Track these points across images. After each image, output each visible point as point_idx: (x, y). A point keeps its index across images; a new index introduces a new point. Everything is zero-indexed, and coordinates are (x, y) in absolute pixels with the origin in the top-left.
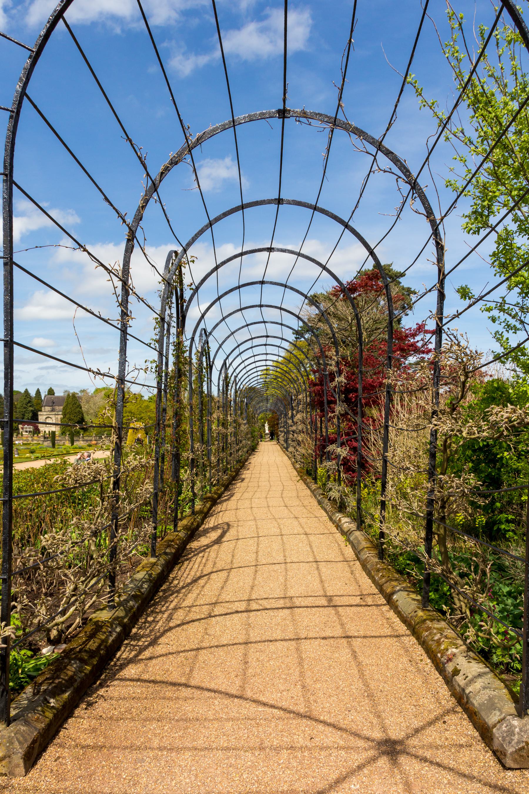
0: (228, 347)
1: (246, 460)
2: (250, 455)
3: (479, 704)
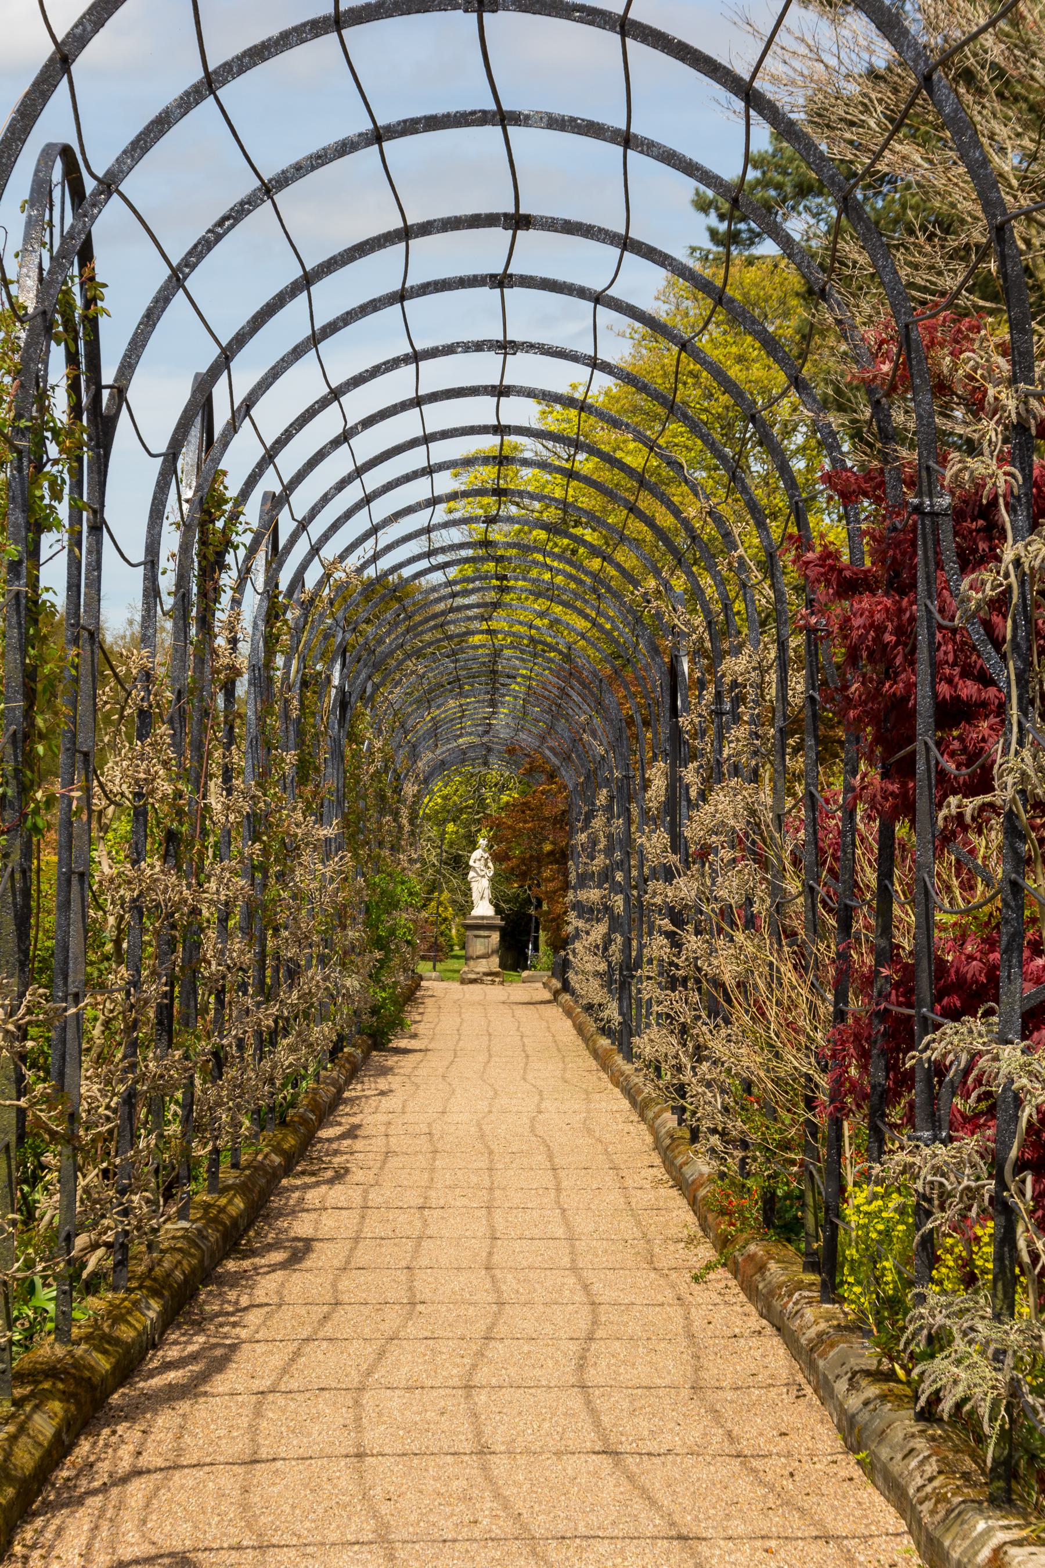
1: (326, 1110)
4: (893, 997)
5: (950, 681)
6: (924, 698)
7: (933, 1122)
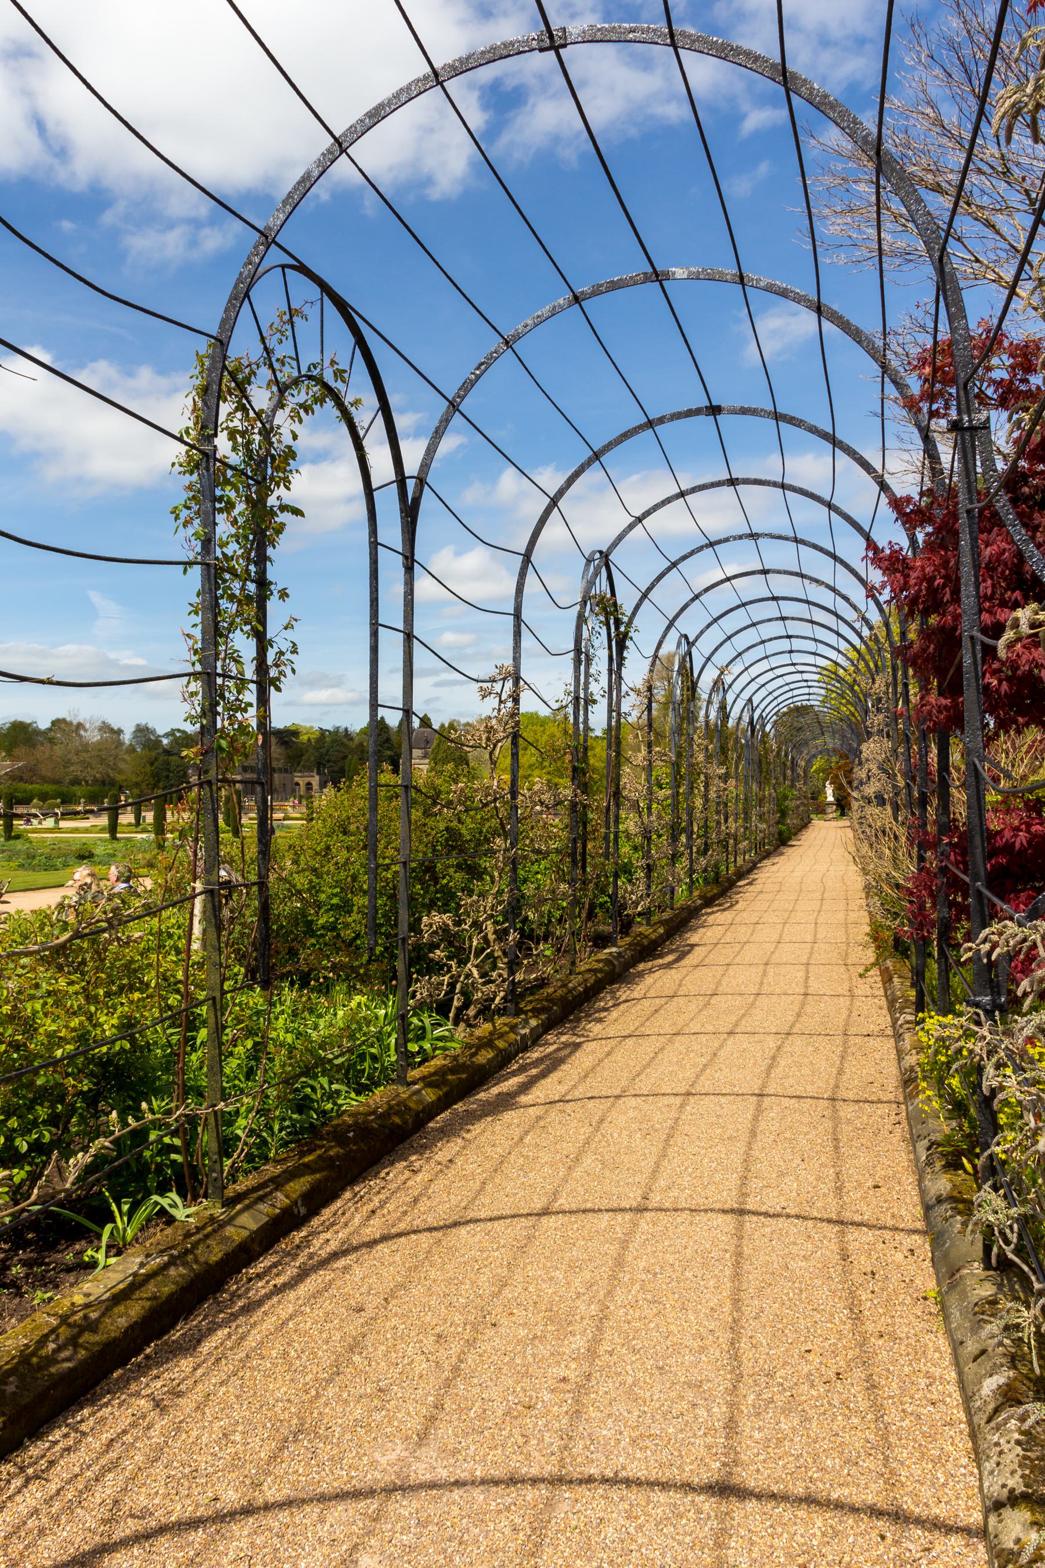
0: (722, 657)
2: (768, 855)
3: (252, 989)
4: (952, 857)
5: (989, 611)
6: (968, 597)
7: (992, 988)
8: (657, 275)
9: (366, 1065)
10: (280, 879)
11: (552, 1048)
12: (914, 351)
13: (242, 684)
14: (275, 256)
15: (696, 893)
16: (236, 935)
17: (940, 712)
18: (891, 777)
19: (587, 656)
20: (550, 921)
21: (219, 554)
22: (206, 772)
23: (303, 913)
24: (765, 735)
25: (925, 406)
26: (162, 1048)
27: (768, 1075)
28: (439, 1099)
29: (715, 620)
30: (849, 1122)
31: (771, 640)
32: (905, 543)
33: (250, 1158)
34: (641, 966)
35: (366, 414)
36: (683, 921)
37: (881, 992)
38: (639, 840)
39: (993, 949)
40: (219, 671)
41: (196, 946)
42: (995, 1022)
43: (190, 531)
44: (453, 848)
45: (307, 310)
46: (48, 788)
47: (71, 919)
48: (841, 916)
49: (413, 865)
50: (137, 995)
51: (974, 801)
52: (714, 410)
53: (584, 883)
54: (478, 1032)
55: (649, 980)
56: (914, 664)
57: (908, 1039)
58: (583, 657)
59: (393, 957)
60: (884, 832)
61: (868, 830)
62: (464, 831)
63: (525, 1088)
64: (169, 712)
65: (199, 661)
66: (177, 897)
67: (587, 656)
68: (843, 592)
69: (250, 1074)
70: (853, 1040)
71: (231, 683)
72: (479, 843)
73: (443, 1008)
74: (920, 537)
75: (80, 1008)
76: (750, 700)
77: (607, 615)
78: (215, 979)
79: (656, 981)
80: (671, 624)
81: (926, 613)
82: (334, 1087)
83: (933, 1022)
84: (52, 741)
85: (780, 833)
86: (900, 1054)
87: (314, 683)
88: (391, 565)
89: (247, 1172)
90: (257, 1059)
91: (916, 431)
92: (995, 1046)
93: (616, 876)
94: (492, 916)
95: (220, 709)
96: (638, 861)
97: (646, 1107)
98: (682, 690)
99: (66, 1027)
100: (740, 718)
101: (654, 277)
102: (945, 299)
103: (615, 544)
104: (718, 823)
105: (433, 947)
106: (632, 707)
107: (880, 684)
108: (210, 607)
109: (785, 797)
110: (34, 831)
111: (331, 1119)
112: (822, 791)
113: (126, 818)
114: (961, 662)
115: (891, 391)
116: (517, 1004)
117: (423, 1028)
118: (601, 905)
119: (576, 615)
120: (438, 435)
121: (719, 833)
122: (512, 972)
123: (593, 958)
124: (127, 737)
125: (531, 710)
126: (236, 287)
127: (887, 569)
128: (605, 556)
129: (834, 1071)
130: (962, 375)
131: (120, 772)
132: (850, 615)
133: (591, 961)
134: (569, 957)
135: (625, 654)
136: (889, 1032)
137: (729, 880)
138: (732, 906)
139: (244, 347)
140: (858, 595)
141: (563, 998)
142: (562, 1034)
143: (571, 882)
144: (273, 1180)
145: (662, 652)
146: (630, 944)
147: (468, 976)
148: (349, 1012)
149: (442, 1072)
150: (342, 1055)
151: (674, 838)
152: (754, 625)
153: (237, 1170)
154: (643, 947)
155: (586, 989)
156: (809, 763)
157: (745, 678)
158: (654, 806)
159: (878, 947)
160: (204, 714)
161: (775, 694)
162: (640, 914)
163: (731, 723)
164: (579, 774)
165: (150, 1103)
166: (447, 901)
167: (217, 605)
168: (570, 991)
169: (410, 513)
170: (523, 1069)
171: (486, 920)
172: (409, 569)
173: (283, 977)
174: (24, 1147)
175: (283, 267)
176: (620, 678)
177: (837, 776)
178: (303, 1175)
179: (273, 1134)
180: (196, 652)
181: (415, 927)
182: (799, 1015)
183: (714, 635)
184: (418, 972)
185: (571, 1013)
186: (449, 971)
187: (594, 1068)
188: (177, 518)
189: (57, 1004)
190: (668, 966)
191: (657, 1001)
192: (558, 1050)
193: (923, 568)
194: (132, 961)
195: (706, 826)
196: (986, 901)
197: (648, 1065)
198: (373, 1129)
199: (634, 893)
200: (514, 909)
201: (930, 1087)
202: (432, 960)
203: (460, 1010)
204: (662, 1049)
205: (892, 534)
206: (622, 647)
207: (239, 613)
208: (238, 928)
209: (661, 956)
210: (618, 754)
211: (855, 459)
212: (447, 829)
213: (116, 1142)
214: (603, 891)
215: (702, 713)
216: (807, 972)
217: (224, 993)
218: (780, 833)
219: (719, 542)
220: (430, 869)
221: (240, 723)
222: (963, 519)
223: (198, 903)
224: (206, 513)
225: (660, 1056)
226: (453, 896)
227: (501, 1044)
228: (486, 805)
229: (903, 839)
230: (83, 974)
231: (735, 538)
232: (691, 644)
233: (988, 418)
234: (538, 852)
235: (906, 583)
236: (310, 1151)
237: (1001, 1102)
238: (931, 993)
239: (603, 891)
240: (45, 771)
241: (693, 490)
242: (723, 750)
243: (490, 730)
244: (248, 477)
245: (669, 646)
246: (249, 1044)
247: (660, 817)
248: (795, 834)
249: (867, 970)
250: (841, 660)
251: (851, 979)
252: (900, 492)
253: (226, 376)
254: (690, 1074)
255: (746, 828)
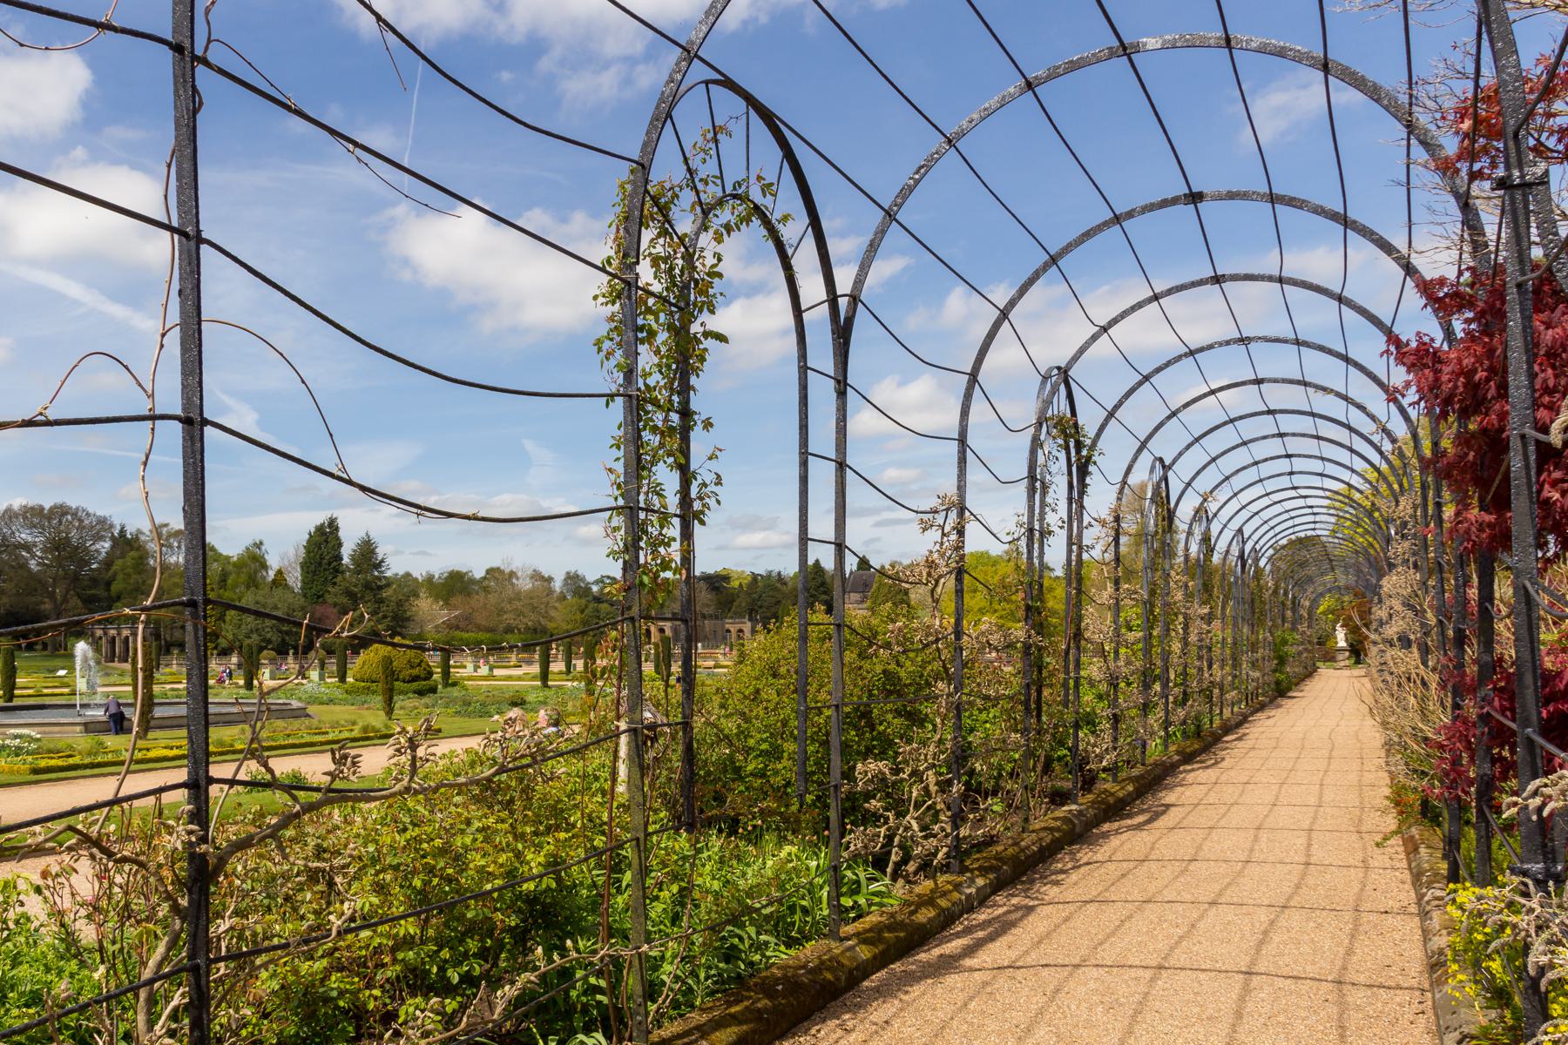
0: (1205, 483)
2: (1262, 707)
4: (1497, 703)
6: (1518, 388)
7: (1545, 855)
8: (1125, 49)
9: (797, 917)
10: (708, 723)
11: (1001, 911)
12: (1449, 103)
13: (664, 518)
14: (698, 72)
15: (1173, 748)
16: (662, 779)
17: (1481, 530)
18: (1419, 613)
19: (1043, 483)
20: (1000, 775)
21: (641, 385)
22: (629, 608)
23: (731, 758)
24: (1259, 572)
25: (1464, 167)
26: (589, 889)
27: (1258, 951)
28: (875, 957)
29: (1197, 440)
30: (1359, 1008)
31: (1266, 460)
32: (1439, 336)
33: (676, 1005)
34: (1106, 827)
35: (794, 229)
36: (1156, 779)
37: (1404, 864)
38: (1103, 687)
39: (1544, 805)
40: (642, 505)
41: (621, 789)
42: (1549, 893)
43: (613, 362)
44: (890, 693)
45: (731, 126)
46: (481, 636)
47: (497, 752)
48: (1353, 777)
49: (847, 709)
50: (562, 835)
51: (1524, 632)
52: (1195, 198)
53: (1039, 733)
54: (918, 889)
55: (1115, 842)
56: (1448, 476)
57: (1436, 919)
58: (1038, 484)
59: (826, 806)
60: (1409, 679)
61: (1389, 678)
62: (903, 674)
63: (970, 951)
64: (590, 554)
65: (622, 495)
66: (603, 737)
67: (1043, 483)
68: (1358, 400)
69: (676, 919)
70: (1365, 917)
71: (654, 518)
72: (920, 688)
73: (880, 863)
74: (1458, 326)
75: (508, 845)
76: (1240, 531)
77: (1066, 437)
78: (639, 819)
79: (1123, 844)
80: (1143, 445)
81: (1464, 414)
82: (763, 938)
83: (1467, 895)
84: (486, 589)
85: (1278, 683)
86: (1426, 934)
87: (748, 525)
88: (822, 391)
89: (671, 1019)
90: (683, 905)
91: (1453, 200)
92: (1547, 920)
93: (1077, 726)
94: (934, 766)
95: (642, 544)
96: (1103, 710)
97: (1109, 979)
98: (1156, 521)
99: (495, 862)
100: (1227, 552)
101: (1121, 52)
102: (1489, 33)
103: (1075, 358)
104: (1200, 669)
105: (868, 796)
106: (1097, 543)
107: (1405, 506)
108: (633, 441)
109: (1285, 642)
110: (470, 678)
111: (759, 971)
112: (1331, 635)
113: (557, 666)
114: (1509, 467)
115: (1419, 154)
116: (962, 862)
117: (858, 882)
118: (1060, 759)
119: (1029, 439)
120: (873, 248)
121: (1200, 681)
122: (956, 827)
123: (1050, 815)
124: (557, 585)
125: (981, 548)
126: (657, 107)
127: (1413, 365)
128: (1064, 372)
129: (1342, 951)
130: (1512, 122)
131: (551, 619)
132: (1367, 427)
133: (1046, 819)
134: (1021, 814)
135: (1088, 480)
136: (1413, 909)
137: (1213, 734)
138: (1217, 763)
139: (667, 170)
140: (1376, 402)
141: (1014, 858)
142: (1013, 895)
143: (1025, 731)
144: (698, 1028)
145: (1131, 480)
146: (1093, 802)
147: (907, 829)
148: (780, 862)
149: (878, 929)
150: (770, 904)
151: (1147, 686)
152: (1245, 443)
153: (663, 1015)
154: (1109, 805)
155: (1041, 849)
156: (1315, 603)
157: (1234, 506)
158: (1122, 650)
159: (1401, 813)
160: (626, 550)
161: (1272, 523)
162: (1105, 770)
163: (1216, 558)
164: (1034, 614)
165: (575, 942)
166: (884, 748)
167: (640, 437)
168: (1022, 850)
169: (842, 333)
170: (968, 931)
171: (927, 769)
172: (842, 394)
173: (709, 823)
174: (456, 979)
175: (707, 83)
176: (1082, 507)
177: (1350, 618)
178: (729, 1026)
179: (698, 982)
180: (619, 487)
181: (848, 775)
182: (1298, 887)
183: (1196, 458)
184: (852, 823)
185: (1024, 874)
186: (886, 823)
187: (1048, 934)
188: (600, 350)
189: (486, 840)
190: (1139, 827)
191: (1125, 865)
192: (1009, 912)
193: (1460, 361)
194: (560, 801)
195: (1185, 673)
196: (1538, 751)
197: (1113, 933)
198: (803, 983)
199: (1099, 746)
200: (961, 756)
201: (1462, 969)
202: (868, 811)
203: (898, 865)
204: (1130, 917)
205: (1419, 322)
206: (1083, 472)
207: (662, 445)
208: (665, 773)
209: (1130, 816)
210: (1079, 591)
211: (1373, 241)
212: (884, 672)
213: (543, 977)
214: (1062, 743)
215: (1181, 545)
216: (1310, 839)
217: (648, 835)
218: (1278, 683)
219: (1201, 350)
220: (866, 715)
221: (663, 559)
222: (1512, 295)
223: (624, 739)
224: (628, 343)
225: (1127, 925)
226: (891, 744)
227: (943, 903)
228: (927, 645)
229: (1433, 686)
230: (512, 813)
231: (1220, 344)
232: (1166, 468)
233: (1547, 172)
234: (986, 698)
235: (1437, 379)
236: (737, 1002)
237: (1551, 982)
238: (1468, 866)
239: (1062, 743)
240: (480, 619)
241: (1170, 292)
242: (1207, 588)
243: (931, 564)
244: (671, 304)
245: (1140, 475)
246: (675, 888)
247: (1128, 663)
248: (1297, 684)
249: (1385, 839)
250: (1356, 481)
251: (1365, 849)
252: (1429, 274)
253: (649, 203)
254: (1162, 945)
255: (1235, 677)
